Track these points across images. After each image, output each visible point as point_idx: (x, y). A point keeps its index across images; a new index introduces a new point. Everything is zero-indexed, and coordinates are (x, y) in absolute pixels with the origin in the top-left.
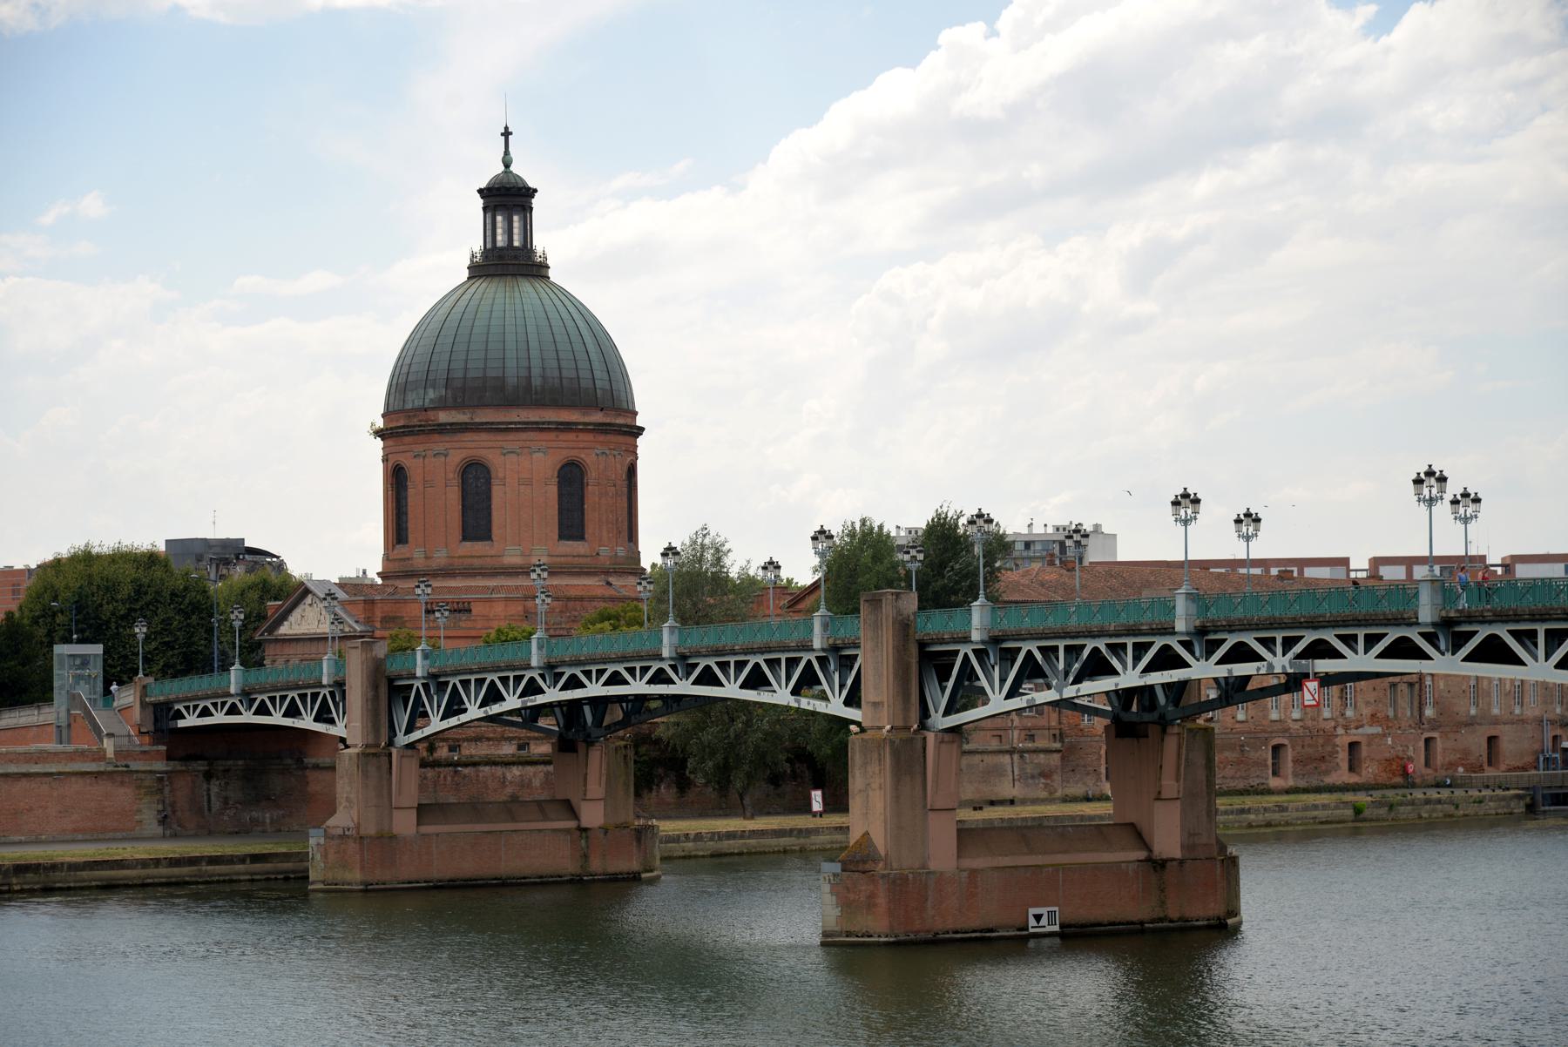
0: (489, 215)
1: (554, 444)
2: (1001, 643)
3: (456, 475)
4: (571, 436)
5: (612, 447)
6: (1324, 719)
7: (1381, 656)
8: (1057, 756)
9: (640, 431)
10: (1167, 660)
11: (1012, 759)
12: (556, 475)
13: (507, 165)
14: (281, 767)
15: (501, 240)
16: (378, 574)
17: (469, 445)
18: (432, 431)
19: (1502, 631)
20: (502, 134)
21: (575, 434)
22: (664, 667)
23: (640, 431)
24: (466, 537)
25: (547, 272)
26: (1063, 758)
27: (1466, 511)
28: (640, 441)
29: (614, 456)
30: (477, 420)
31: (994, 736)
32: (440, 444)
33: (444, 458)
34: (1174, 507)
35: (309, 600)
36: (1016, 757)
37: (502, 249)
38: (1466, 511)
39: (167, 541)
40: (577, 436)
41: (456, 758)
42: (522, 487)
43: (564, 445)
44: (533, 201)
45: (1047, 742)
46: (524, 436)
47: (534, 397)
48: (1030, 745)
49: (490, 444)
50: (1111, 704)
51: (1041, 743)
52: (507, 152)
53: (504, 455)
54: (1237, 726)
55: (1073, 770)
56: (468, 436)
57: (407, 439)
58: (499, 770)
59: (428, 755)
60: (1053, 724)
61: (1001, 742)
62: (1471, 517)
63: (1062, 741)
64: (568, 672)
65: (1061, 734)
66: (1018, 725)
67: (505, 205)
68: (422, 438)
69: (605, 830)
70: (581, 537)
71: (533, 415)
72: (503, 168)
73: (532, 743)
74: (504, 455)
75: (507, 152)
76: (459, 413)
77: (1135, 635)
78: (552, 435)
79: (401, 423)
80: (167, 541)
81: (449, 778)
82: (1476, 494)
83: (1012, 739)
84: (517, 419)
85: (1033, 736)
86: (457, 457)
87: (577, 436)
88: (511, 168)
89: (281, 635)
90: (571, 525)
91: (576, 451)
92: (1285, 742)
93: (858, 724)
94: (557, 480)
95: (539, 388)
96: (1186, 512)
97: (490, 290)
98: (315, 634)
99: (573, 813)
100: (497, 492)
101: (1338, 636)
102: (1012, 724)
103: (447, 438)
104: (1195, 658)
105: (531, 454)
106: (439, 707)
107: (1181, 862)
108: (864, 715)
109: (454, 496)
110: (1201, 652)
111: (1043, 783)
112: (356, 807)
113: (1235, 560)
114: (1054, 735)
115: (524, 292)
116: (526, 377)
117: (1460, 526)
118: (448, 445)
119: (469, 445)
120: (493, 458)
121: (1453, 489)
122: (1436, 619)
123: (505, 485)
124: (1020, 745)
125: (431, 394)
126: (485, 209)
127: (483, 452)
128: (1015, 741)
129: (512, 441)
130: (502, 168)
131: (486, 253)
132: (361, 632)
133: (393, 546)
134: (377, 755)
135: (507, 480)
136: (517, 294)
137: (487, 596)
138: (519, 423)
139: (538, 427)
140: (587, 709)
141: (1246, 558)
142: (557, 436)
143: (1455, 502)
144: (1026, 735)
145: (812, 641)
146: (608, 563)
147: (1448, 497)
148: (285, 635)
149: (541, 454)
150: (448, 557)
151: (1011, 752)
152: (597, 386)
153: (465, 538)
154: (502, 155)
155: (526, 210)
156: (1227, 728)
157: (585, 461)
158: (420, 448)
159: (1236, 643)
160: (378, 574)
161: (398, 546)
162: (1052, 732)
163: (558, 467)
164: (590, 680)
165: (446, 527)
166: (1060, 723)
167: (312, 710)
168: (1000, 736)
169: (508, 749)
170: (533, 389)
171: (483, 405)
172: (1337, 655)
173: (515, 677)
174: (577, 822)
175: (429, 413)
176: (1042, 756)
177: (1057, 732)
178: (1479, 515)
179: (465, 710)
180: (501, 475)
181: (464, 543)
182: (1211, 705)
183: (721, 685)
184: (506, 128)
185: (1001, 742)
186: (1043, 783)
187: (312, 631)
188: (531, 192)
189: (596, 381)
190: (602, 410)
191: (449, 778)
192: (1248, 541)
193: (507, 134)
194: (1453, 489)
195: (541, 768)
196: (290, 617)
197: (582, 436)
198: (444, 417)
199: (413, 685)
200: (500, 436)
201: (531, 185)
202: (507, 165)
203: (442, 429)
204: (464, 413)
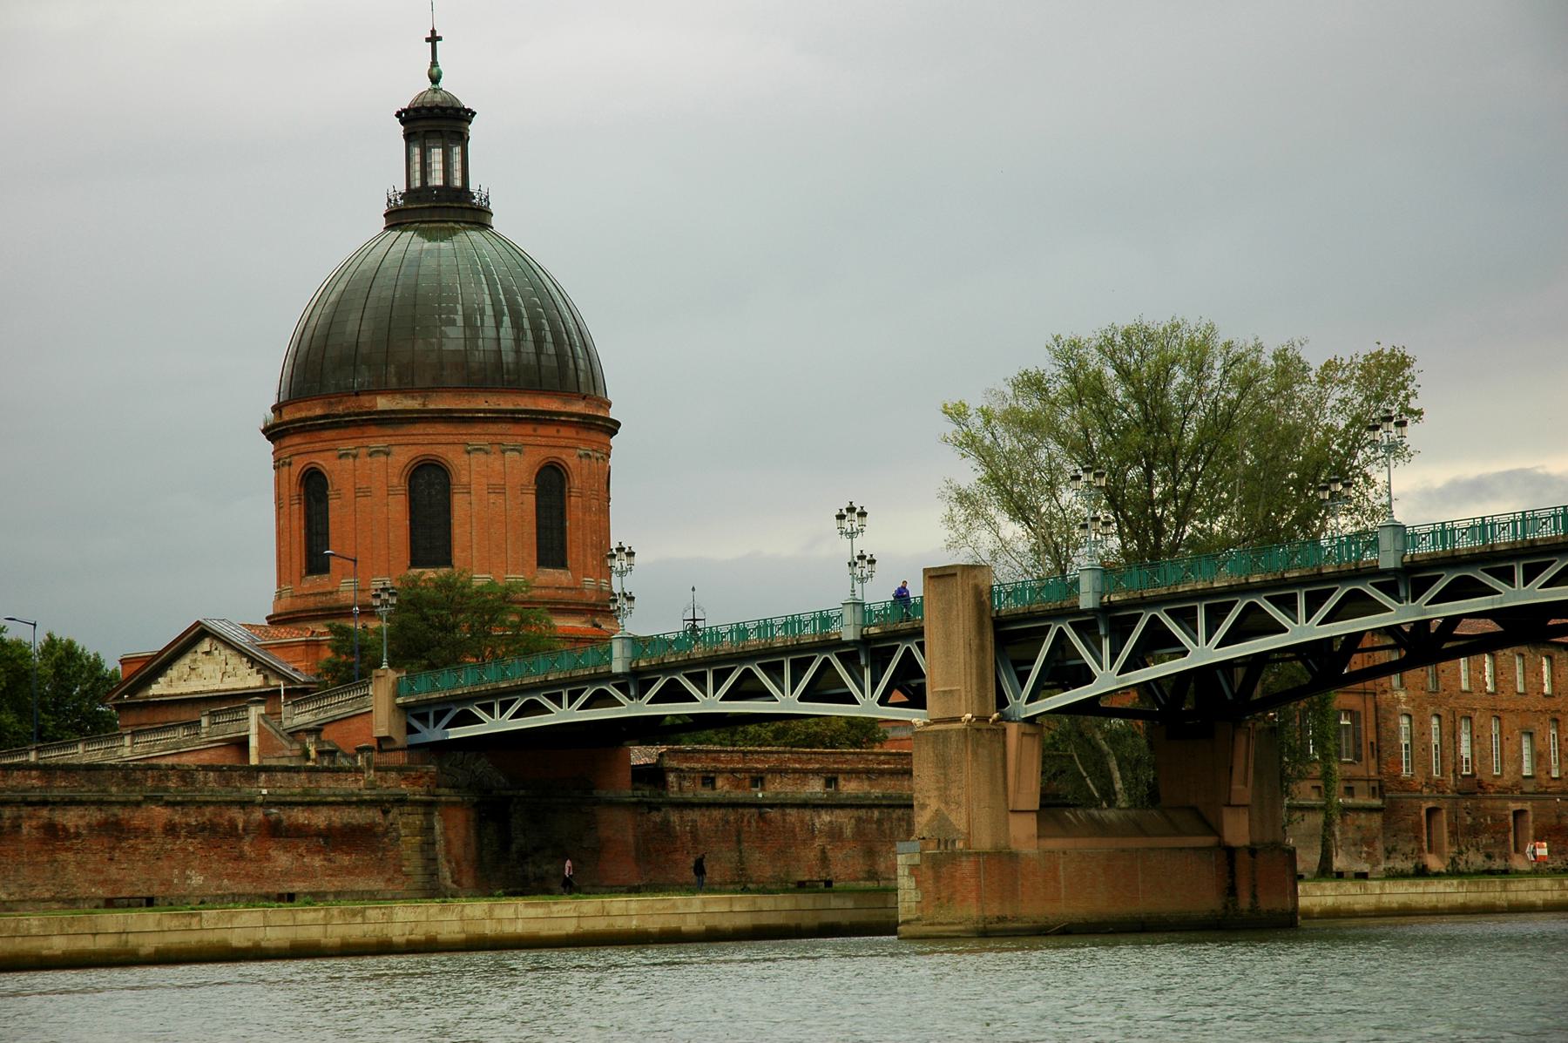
1: (530, 440)
3: (403, 481)
4: (551, 430)
5: (595, 447)
8: (1377, 820)
9: (612, 428)
13: (435, 79)
14: (569, 800)
15: (437, 180)
17: (420, 439)
18: (367, 423)
20: (428, 40)
21: (555, 429)
23: (612, 428)
26: (1386, 820)
29: (597, 459)
30: (432, 407)
31: (1313, 787)
32: (378, 439)
33: (351, 460)
35: (206, 645)
40: (558, 431)
41: (760, 795)
42: (492, 496)
43: (544, 441)
46: (493, 428)
47: (505, 376)
48: (1350, 801)
49: (451, 439)
51: (1361, 800)
52: (434, 63)
53: (469, 452)
54: (1552, 784)
56: (419, 429)
57: (327, 434)
58: (807, 814)
60: (1372, 774)
63: (1382, 797)
65: (1381, 787)
67: (440, 131)
68: (350, 432)
69: (1252, 851)
70: (561, 563)
71: (506, 403)
72: (429, 84)
73: (841, 777)
74: (469, 452)
75: (434, 63)
76: (405, 397)
78: (528, 429)
79: (318, 412)
81: (754, 824)
84: (485, 406)
85: (1351, 788)
86: (402, 457)
87: (558, 431)
88: (442, 84)
89: (154, 696)
90: (552, 551)
91: (556, 450)
95: (511, 366)
97: (409, 242)
99: (1214, 829)
100: (459, 503)
103: (390, 432)
105: (503, 452)
109: (398, 509)
111: (1366, 852)
112: (963, 811)
114: (1374, 788)
116: (494, 351)
118: (392, 440)
119: (420, 439)
120: (455, 458)
126: (408, 137)
127: (439, 450)
129: (478, 436)
131: (410, 194)
132: (305, 683)
133: (302, 577)
135: (473, 486)
138: (490, 411)
139: (513, 417)
140: (1219, 673)
142: (535, 430)
146: (594, 598)
149: (515, 453)
155: (462, 139)
156: (1541, 787)
158: (348, 446)
162: (1372, 784)
163: (537, 470)
164: (1192, 632)
165: (389, 548)
166: (1379, 773)
169: (815, 787)
170: (505, 366)
171: (438, 388)
174: (1216, 838)
175: (361, 397)
177: (1376, 784)
180: (465, 480)
183: (853, 701)
184: (433, 32)
186: (1366, 852)
187: (211, 688)
190: (584, 398)
191: (754, 824)
193: (434, 39)
196: (169, 672)
197: (565, 431)
200: (462, 429)
202: (435, 79)
204: (413, 398)
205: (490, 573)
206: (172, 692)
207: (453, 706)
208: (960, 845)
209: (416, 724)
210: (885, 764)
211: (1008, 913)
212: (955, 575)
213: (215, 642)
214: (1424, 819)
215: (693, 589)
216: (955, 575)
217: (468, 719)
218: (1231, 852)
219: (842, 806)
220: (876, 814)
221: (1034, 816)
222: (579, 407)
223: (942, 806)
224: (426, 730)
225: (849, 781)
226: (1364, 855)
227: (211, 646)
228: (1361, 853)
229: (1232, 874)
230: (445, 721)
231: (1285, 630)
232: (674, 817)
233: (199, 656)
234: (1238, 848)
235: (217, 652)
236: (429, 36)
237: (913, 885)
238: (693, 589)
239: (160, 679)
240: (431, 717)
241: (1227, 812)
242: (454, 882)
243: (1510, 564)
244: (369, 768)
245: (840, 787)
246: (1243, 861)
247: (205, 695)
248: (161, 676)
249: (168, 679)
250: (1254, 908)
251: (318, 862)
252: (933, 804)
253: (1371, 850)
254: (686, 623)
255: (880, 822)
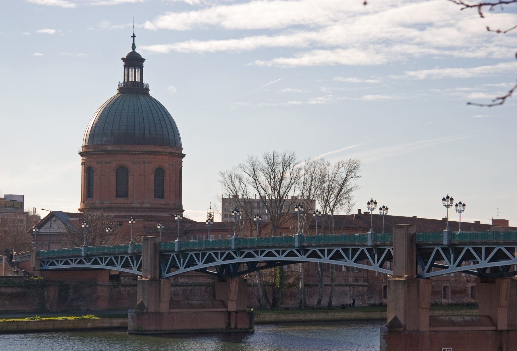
0: (127, 70)
2: (305, 248)
6: (463, 277)
7: (286, 256)
8: (366, 289)
10: (229, 257)
11: (350, 289)
12: (154, 172)
15: (131, 79)
16: (78, 209)
19: (317, 250)
20: (132, 37)
22: (82, 259)
24: (155, 197)
25: (149, 92)
27: (460, 208)
28: (184, 160)
31: (343, 279)
33: (100, 165)
34: (443, 201)
35: (54, 219)
36: (351, 288)
37: (131, 82)
38: (460, 208)
39: (5, 195)
44: (144, 63)
45: (362, 282)
48: (356, 283)
50: (217, 271)
51: (360, 283)
52: (134, 44)
53: (134, 164)
55: (372, 294)
59: (175, 282)
60: (365, 275)
61: (346, 282)
62: (462, 211)
63: (368, 282)
64: (247, 252)
65: (367, 279)
66: (352, 275)
69: (236, 312)
73: (179, 278)
75: (134, 44)
77: (353, 246)
80: (5, 195)
82: (375, 201)
83: (350, 281)
85: (357, 280)
88: (135, 51)
89: (41, 232)
90: (159, 193)
92: (449, 285)
93: (141, 276)
94: (154, 174)
96: (448, 203)
98: (56, 232)
99: (226, 307)
101: (505, 248)
102: (350, 275)
104: (236, 256)
105: (144, 163)
106: (378, 260)
107: (508, 331)
108: (142, 274)
110: (239, 255)
113: (498, 220)
115: (141, 100)
117: (458, 214)
121: (456, 201)
122: (373, 245)
123: (134, 175)
124: (353, 283)
125: (105, 139)
126: (125, 67)
128: (351, 282)
130: (131, 50)
134: (156, 281)
136: (139, 100)
137: (126, 219)
138: (140, 151)
139: (148, 153)
141: (459, 221)
143: (457, 205)
144: (355, 279)
145: (442, 241)
147: (454, 204)
148: (42, 232)
150: (110, 203)
151: (350, 285)
152: (170, 138)
153: (117, 196)
154: (132, 45)
155: (141, 67)
157: (164, 167)
159: (498, 249)
160: (78, 209)
161: (88, 198)
162: (364, 278)
163: (155, 169)
167: (378, 260)
168: (346, 280)
172: (274, 256)
173: (61, 260)
176: (361, 288)
177: (366, 278)
178: (465, 210)
179: (197, 265)
181: (116, 198)
182: (245, 272)
184: (134, 34)
185: (346, 282)
186: (361, 298)
187: (55, 231)
188: (143, 60)
189: (169, 136)
190: (171, 147)
192: (460, 213)
193: (134, 36)
194: (456, 201)
195: (181, 287)
196: (45, 226)
198: (109, 148)
199: (171, 254)
201: (143, 56)
203: (109, 153)
204: (118, 147)
205: (139, 199)
206: (45, 232)
207: (50, 260)
208: (145, 311)
209: (43, 264)
210: (194, 274)
211: (158, 329)
212: (149, 239)
213: (56, 218)
214: (383, 289)
215: (211, 203)
216: (149, 239)
217: (53, 264)
218: (229, 313)
219: (179, 286)
220: (190, 288)
221: (169, 303)
222: (170, 150)
223: (143, 300)
224: (44, 266)
225: (182, 279)
226: (360, 299)
227: (55, 219)
228: (359, 299)
229: (229, 318)
230: (49, 264)
231: (322, 258)
232: (122, 289)
233: (53, 222)
234: (232, 312)
235: (57, 221)
236: (132, 35)
237: (132, 321)
238: (211, 203)
239: (42, 228)
240: (59, 261)
241: (229, 302)
242: (50, 307)
243: (481, 247)
244: (25, 277)
245: (178, 281)
246: (233, 316)
247: (53, 233)
248: (43, 227)
249: (44, 228)
250: (236, 328)
251: (7, 303)
252: (141, 300)
253: (363, 298)
254: (208, 213)
255: (191, 290)
